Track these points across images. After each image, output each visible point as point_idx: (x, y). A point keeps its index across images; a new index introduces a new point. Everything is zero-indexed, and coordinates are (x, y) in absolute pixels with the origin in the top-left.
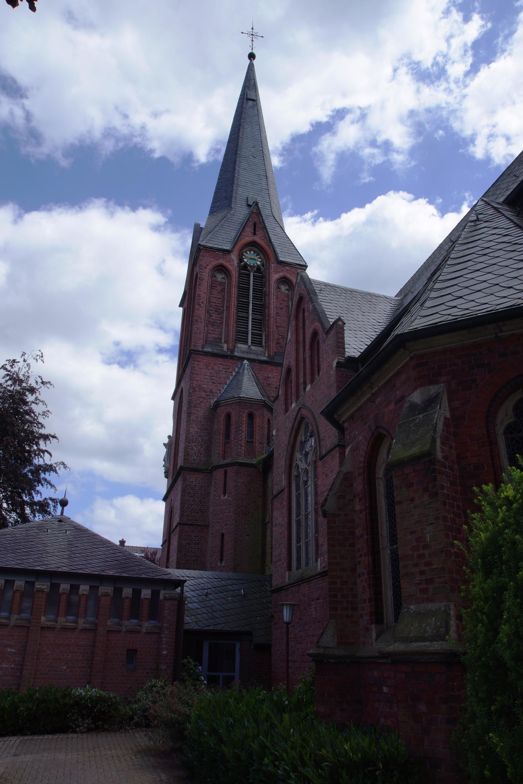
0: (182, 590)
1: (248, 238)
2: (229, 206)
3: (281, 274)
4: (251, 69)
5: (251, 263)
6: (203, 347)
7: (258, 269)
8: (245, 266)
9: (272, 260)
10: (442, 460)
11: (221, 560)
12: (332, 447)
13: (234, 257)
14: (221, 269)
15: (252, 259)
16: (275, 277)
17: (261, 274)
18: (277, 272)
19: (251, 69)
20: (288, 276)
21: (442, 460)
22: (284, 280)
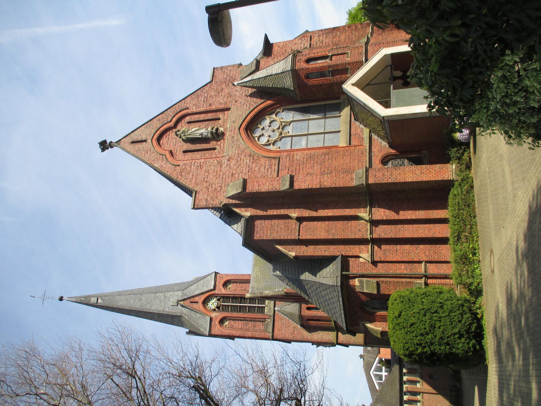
0: (509, 55)
1: (200, 306)
2: (180, 317)
3: (222, 287)
4: (85, 302)
5: (215, 304)
6: (270, 333)
7: (218, 300)
8: (218, 307)
9: (213, 292)
10: (303, 78)
11: (219, 119)
12: (196, 153)
13: (214, 315)
14: (222, 321)
15: (213, 304)
16: (223, 291)
17: (225, 298)
18: (220, 290)
19: (85, 302)
20: (222, 283)
21: (303, 78)
22: (225, 284)
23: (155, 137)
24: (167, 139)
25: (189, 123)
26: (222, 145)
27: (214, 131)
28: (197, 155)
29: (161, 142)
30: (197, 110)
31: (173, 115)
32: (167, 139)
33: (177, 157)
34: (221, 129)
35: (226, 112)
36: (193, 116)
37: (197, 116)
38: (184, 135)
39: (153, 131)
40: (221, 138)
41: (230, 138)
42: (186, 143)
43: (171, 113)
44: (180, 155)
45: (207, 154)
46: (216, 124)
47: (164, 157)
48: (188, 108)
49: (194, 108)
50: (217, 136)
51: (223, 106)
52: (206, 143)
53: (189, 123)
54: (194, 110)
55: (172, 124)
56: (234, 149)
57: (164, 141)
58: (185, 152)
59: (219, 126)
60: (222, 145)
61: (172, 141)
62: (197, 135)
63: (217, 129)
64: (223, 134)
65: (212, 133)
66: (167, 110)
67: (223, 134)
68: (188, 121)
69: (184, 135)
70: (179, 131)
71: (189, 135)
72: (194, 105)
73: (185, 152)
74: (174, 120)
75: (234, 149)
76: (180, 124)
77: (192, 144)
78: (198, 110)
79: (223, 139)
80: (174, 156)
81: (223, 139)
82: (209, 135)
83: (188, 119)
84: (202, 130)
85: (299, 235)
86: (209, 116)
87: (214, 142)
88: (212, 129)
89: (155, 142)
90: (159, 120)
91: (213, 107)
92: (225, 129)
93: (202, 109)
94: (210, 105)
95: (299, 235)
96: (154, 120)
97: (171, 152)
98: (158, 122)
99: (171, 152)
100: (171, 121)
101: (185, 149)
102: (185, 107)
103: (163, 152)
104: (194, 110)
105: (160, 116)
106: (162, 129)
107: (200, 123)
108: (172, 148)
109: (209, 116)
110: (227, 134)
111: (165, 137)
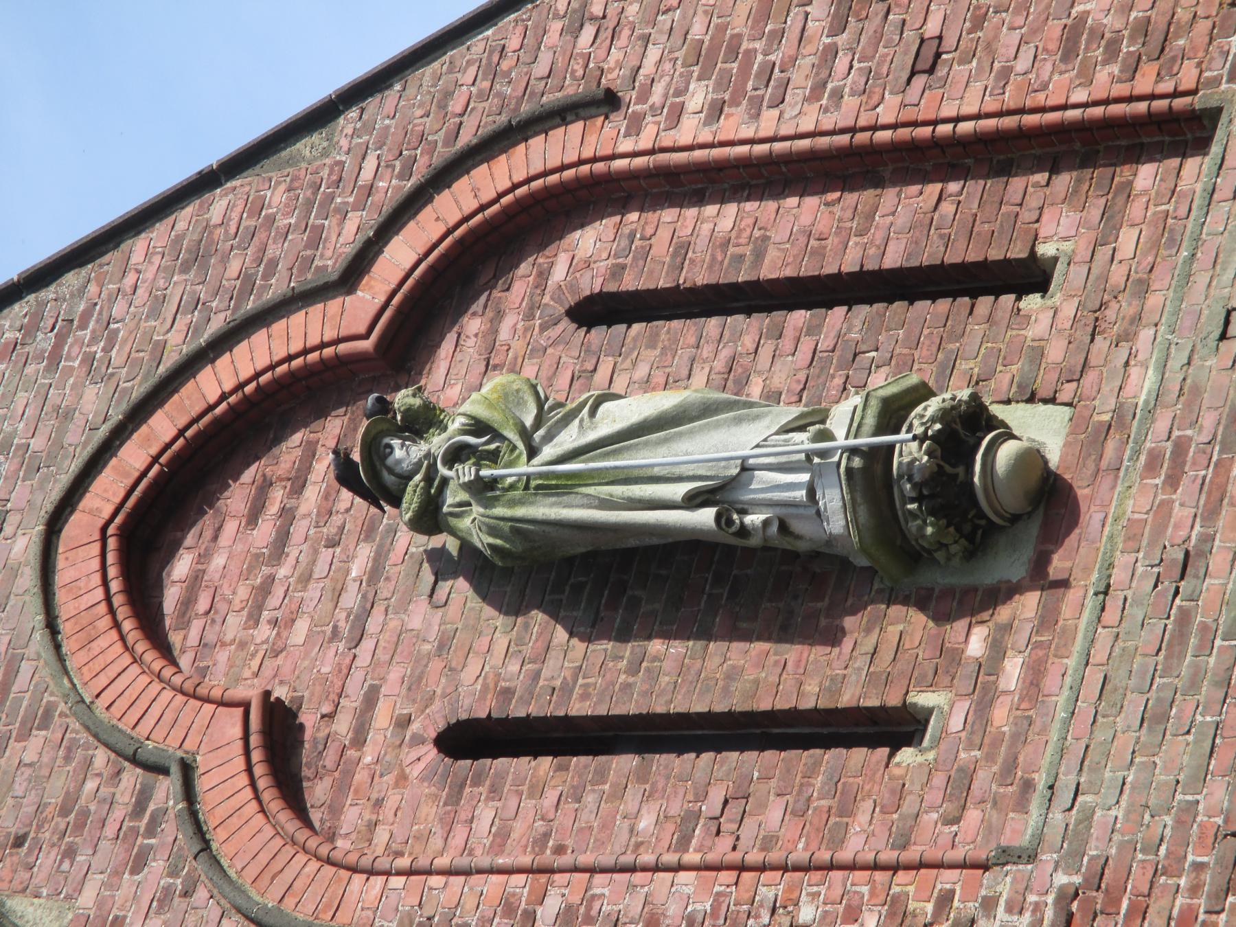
11: (1031, 276)
12: (623, 764)
23: (107, 493)
24: (265, 530)
25: (597, 311)
26: (1013, 670)
27: (909, 450)
28: (637, 802)
29: (182, 566)
30: (736, 125)
31: (391, 189)
32: (265, 530)
33: (352, 817)
34: (1040, 430)
35: (1146, 175)
36: (668, 225)
37: (724, 217)
38: (483, 489)
39: (96, 406)
40: (1010, 564)
41: (1134, 573)
42: (514, 607)
43: (373, 164)
44: (388, 785)
45: (776, 795)
46: (959, 352)
47: (166, 790)
48: (609, 101)
49: (698, 96)
50: (956, 523)
51: (1106, 79)
52: (784, 631)
53: (597, 311)
54: (689, 130)
55: (355, 317)
56: (1179, 752)
57: (214, 558)
58: (469, 741)
59: (1002, 381)
60: (1013, 670)
61: (315, 589)
62: (659, 494)
63: (969, 426)
64: (1050, 501)
65: (871, 473)
66: (321, 116)
67: (1050, 501)
68: (591, 283)
69: (483, 489)
70: (421, 422)
71: (555, 486)
72: (702, 58)
73: (469, 741)
74: (402, 255)
75: (1179, 752)
76: (473, 325)
77: (588, 627)
78: (747, 130)
79: (1039, 576)
80: (317, 792)
81: (1039, 576)
82: (836, 513)
83: (589, 253)
84: (739, 431)
85: (461, 209)
86: (899, 224)
87: (907, 625)
88: (893, 414)
89: (83, 567)
90: (197, 257)
91: (964, 99)
92: (1091, 437)
93: (798, 120)
94: (928, 61)
95: (461, 209)
96: (138, 247)
97: (279, 738)
98: (179, 287)
99: (279, 738)
100: (353, 273)
101: (474, 703)
102: (572, 89)
103: (165, 722)
104: (691, 120)
105: (219, 204)
106: (212, 384)
107: (746, 329)
108: (301, 670)
109: (899, 224)
110: (1117, 517)
111: (236, 498)
